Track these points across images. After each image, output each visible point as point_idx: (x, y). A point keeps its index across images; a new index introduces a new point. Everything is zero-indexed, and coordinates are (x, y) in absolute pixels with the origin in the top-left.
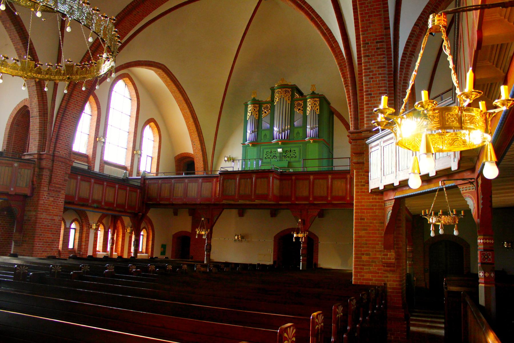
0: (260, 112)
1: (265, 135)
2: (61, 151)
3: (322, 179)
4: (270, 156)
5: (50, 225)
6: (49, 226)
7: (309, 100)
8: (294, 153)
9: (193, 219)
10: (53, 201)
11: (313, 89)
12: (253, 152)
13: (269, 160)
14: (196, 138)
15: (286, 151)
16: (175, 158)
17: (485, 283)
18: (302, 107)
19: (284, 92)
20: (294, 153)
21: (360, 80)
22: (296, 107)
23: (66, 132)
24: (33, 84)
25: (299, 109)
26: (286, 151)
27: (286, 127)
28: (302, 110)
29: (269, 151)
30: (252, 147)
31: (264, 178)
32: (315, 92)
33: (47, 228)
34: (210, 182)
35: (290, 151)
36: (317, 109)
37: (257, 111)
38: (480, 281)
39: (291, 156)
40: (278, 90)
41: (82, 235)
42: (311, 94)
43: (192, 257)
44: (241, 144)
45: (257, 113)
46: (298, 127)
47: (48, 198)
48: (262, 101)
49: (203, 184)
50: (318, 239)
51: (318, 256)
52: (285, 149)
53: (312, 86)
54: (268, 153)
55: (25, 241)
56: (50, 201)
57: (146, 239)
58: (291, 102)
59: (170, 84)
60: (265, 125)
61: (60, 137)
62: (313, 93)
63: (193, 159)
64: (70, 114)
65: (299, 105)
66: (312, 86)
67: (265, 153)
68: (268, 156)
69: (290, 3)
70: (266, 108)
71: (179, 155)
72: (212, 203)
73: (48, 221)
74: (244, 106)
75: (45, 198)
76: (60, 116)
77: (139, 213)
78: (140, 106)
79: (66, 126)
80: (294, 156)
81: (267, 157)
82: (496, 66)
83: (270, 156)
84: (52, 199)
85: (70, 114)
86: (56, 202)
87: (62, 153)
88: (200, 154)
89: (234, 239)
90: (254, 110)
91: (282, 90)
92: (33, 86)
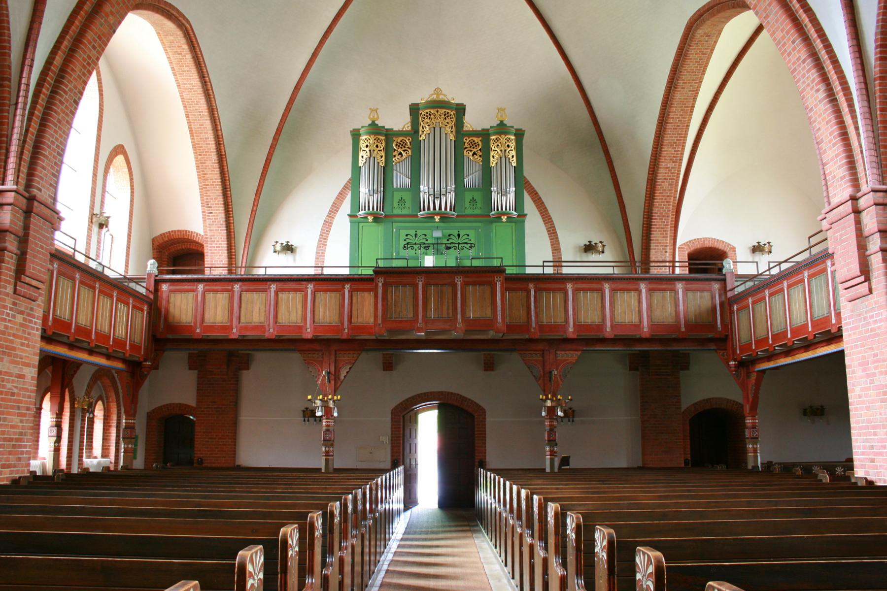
1: (402, 200)
2: (43, 189)
3: (296, 290)
5: (15, 391)
6: (13, 394)
7: (493, 137)
9: (199, 377)
10: (22, 325)
11: (501, 116)
12: (374, 233)
14: (215, 199)
15: (449, 235)
16: (153, 240)
18: (480, 150)
19: (443, 116)
21: (882, 77)
22: (466, 148)
23: (57, 139)
25: (474, 154)
26: (449, 235)
27: (449, 188)
28: (480, 156)
29: (413, 232)
30: (374, 224)
31: (481, 284)
32: (376, 122)
33: (10, 400)
34: (300, 290)
35: (459, 235)
36: (513, 157)
37: (382, 149)
40: (428, 111)
42: (369, 125)
43: (202, 460)
44: (348, 215)
45: (383, 153)
46: (471, 190)
47: (14, 317)
48: (391, 130)
49: (244, 294)
50: (485, 412)
51: (485, 447)
53: (499, 110)
54: (409, 237)
56: (15, 323)
57: (102, 425)
58: (456, 136)
59: (187, 69)
60: (401, 179)
61: (44, 149)
62: (373, 124)
63: (202, 246)
64: (71, 90)
65: (473, 144)
66: (499, 110)
67: (403, 237)
70: (402, 145)
71: (164, 234)
72: (345, 337)
73: (13, 381)
74: (349, 140)
75: (8, 315)
76: (46, 92)
77: (145, 360)
78: (104, 112)
79: (60, 121)
84: (19, 319)
85: (71, 90)
86: (27, 327)
87: (45, 193)
88: (221, 235)
89: (559, 420)
90: (377, 146)
91: (437, 111)
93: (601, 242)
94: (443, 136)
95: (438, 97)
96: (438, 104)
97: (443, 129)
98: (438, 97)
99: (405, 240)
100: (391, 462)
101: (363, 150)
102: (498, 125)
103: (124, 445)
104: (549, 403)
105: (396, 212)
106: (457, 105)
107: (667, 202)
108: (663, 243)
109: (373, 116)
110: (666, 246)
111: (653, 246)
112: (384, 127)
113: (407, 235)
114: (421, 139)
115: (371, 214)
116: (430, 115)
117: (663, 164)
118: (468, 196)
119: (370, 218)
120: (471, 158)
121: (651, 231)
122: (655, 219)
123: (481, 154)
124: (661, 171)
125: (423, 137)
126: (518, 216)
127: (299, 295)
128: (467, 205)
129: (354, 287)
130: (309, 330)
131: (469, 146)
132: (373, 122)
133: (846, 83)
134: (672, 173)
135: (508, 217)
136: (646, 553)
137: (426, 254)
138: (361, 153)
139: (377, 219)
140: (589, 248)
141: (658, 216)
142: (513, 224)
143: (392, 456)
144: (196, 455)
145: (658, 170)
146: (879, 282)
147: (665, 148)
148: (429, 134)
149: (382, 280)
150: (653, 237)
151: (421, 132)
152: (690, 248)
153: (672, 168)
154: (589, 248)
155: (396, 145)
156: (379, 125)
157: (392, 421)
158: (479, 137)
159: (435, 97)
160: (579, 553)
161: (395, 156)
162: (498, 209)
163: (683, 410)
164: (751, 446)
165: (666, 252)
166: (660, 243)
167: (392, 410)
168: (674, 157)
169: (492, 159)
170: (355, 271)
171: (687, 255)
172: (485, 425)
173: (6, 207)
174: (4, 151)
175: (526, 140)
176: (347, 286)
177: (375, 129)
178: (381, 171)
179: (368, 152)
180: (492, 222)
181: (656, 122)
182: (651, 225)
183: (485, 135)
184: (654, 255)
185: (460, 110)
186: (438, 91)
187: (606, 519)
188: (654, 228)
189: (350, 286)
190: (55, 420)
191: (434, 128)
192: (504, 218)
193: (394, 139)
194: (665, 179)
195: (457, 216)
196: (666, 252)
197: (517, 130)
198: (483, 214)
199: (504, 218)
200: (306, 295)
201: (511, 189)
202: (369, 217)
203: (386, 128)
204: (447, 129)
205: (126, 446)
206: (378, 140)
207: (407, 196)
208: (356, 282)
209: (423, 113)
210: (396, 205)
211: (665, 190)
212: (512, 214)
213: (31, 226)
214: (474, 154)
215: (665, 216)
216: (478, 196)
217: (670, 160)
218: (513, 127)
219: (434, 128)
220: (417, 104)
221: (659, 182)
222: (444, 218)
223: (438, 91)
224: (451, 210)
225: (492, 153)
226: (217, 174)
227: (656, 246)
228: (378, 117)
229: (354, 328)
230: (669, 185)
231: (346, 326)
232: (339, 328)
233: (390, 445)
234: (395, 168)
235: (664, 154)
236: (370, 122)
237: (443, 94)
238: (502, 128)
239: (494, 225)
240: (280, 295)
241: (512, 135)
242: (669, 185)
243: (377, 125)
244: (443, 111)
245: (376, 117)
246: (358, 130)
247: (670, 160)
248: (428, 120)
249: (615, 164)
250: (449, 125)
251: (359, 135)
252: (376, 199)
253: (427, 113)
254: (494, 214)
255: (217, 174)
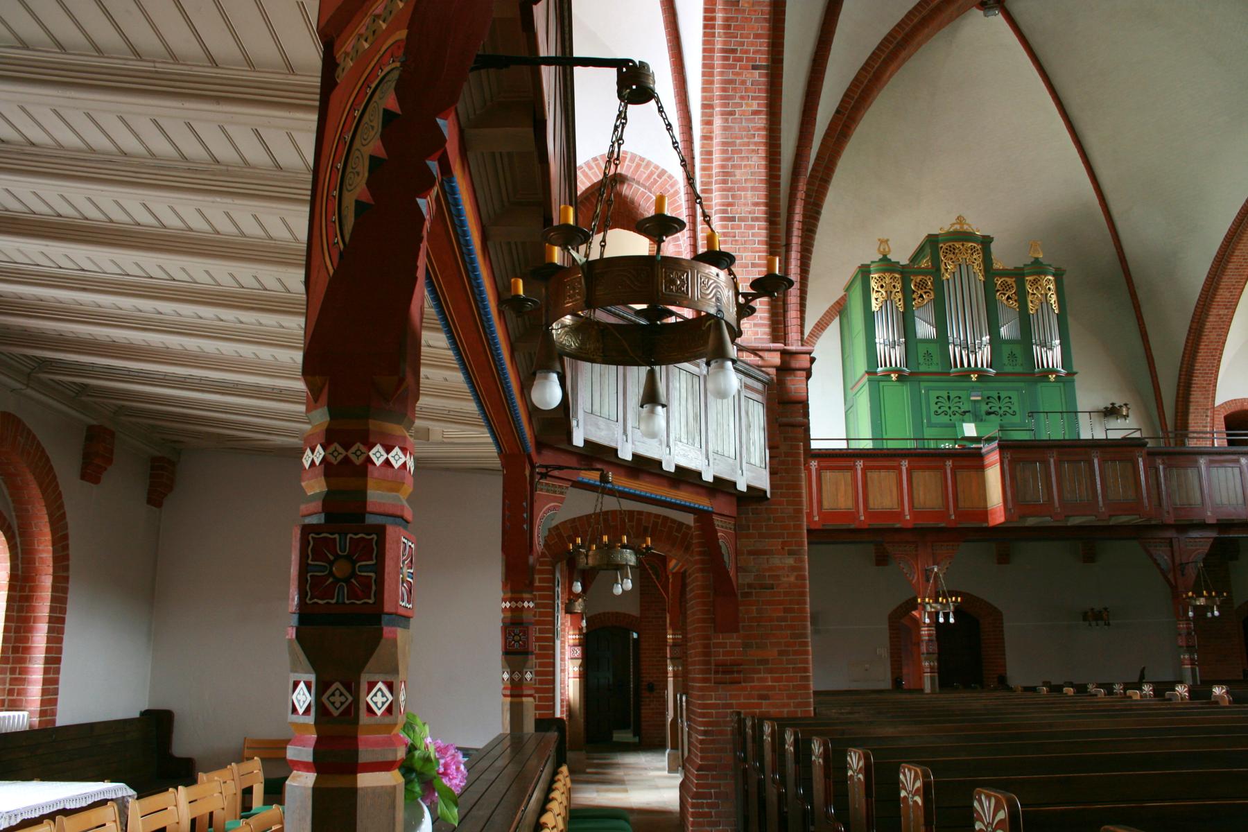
0: (907, 293)
1: (928, 354)
3: (887, 468)
4: (947, 409)
8: (1009, 404)
13: (944, 419)
17: (674, 677)
19: (969, 251)
20: (1009, 404)
22: (998, 291)
24: (755, 108)
28: (1016, 301)
29: (944, 394)
30: (898, 383)
32: (889, 256)
35: (949, 397)
38: (669, 675)
39: (952, 410)
40: (951, 244)
41: (17, 640)
42: (880, 260)
52: (987, 393)
55: (765, 662)
60: (925, 330)
62: (885, 259)
65: (1006, 287)
67: (933, 400)
68: (943, 409)
69: (18, 3)
80: (1011, 411)
81: (940, 411)
82: (509, 243)
83: (947, 409)
92: (755, 113)
93: (1126, 405)
94: (972, 275)
95: (962, 227)
96: (962, 236)
97: (970, 267)
98: (962, 227)
99: (936, 403)
100: (892, 680)
101: (877, 291)
102: (1032, 263)
103: (674, 667)
104: (1201, 602)
105: (923, 368)
106: (984, 237)
107: (1212, 356)
108: (1204, 405)
109: (884, 249)
110: (1207, 409)
111: (1192, 409)
112: (898, 263)
113: (938, 398)
114: (944, 278)
115: (894, 372)
116: (954, 249)
117: (1215, 311)
118: (1006, 350)
119: (894, 376)
120: (1005, 302)
121: (1190, 391)
122: (1197, 377)
123: (1016, 298)
124: (1211, 319)
125: (947, 276)
126: (1067, 374)
127: (848, 475)
128: (1006, 361)
129: (822, 464)
130: (908, 517)
131: (1001, 289)
132: (885, 256)
133: (778, 162)
134: (1223, 322)
135: (1057, 376)
136: (991, 796)
137: (964, 421)
138: (874, 296)
139: (902, 378)
140: (1111, 412)
141: (1200, 373)
142: (1061, 384)
143: (892, 673)
144: (644, 679)
145: (1207, 318)
146: (911, 445)
147: (1221, 292)
148: (954, 273)
149: (1009, 456)
150: (1192, 398)
151: (943, 270)
152: (1226, 411)
153: (1224, 315)
154: (1111, 412)
155: (915, 285)
156: (893, 260)
157: (890, 629)
158: (1012, 278)
159: (958, 227)
160: (869, 799)
161: (915, 299)
162: (891, 365)
163: (1236, 606)
164: (927, 664)
165: (1207, 416)
166: (1200, 406)
167: (889, 615)
168: (1229, 302)
169: (1030, 304)
170: (879, 445)
171: (1223, 419)
172: (1002, 631)
173: (799, 373)
174: (781, 303)
175: (1066, 280)
176: (949, 463)
177: (887, 265)
178: (900, 316)
179: (884, 293)
180: (1036, 382)
181: (1212, 260)
182: (1191, 384)
183: (1018, 275)
184: (1193, 419)
185: (986, 242)
186: (960, 219)
187: (913, 756)
188: (1194, 388)
189: (953, 463)
190: (577, 637)
191: (960, 265)
192: (974, 377)
193: (912, 277)
194: (1213, 328)
195: (996, 374)
196: (1207, 416)
197: (1056, 269)
198: (1025, 371)
199: (1052, 377)
200: (945, 473)
201: (984, 339)
202: (892, 375)
203: (901, 263)
204: (975, 267)
205: (676, 669)
206: (893, 278)
207: (934, 349)
208: (878, 458)
209: (944, 247)
210: (921, 360)
211: (1212, 342)
212: (904, 371)
213: (301, 385)
214: (1009, 298)
215: (1207, 373)
216: (1018, 350)
217: (1224, 305)
218: (1050, 265)
219: (960, 265)
220: (936, 236)
221: (1206, 332)
222: (982, 375)
223: (960, 219)
224: (987, 367)
225: (1030, 298)
226: (762, 325)
227: (1196, 409)
228: (890, 251)
229: (872, 515)
230: (1218, 335)
231: (952, 511)
232: (943, 514)
233: (889, 660)
234: (916, 313)
235: (1218, 298)
236: (881, 256)
237: (968, 224)
238: (1038, 268)
239: (1039, 385)
240: (869, 474)
241: (1049, 275)
242: (1218, 335)
243: (890, 260)
244: (970, 244)
245: (887, 250)
246: (868, 266)
247: (1224, 305)
248: (952, 256)
249: (1143, 310)
250: (977, 262)
251: (869, 273)
252: (897, 355)
253: (950, 247)
254: (883, 371)
255: (762, 325)
